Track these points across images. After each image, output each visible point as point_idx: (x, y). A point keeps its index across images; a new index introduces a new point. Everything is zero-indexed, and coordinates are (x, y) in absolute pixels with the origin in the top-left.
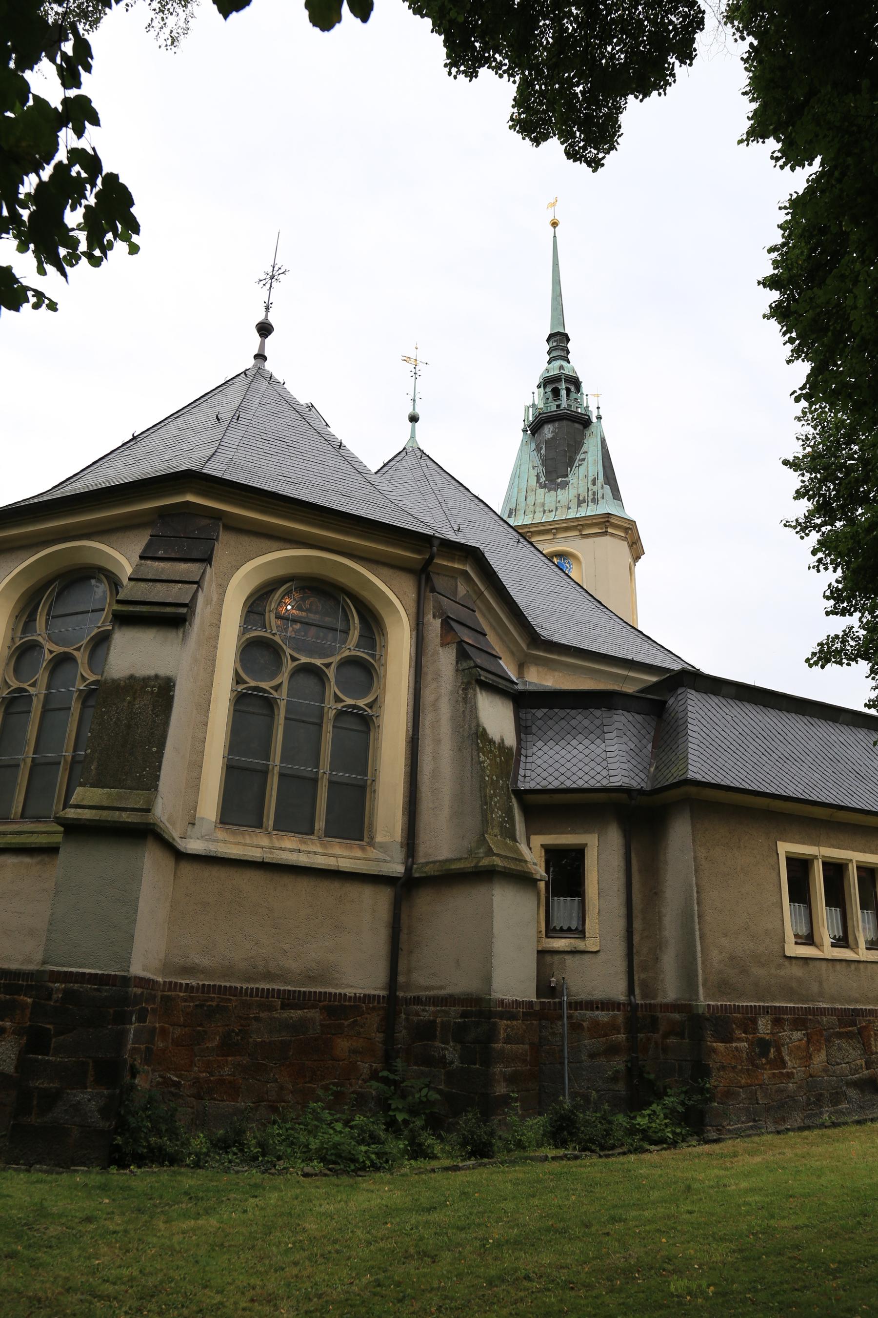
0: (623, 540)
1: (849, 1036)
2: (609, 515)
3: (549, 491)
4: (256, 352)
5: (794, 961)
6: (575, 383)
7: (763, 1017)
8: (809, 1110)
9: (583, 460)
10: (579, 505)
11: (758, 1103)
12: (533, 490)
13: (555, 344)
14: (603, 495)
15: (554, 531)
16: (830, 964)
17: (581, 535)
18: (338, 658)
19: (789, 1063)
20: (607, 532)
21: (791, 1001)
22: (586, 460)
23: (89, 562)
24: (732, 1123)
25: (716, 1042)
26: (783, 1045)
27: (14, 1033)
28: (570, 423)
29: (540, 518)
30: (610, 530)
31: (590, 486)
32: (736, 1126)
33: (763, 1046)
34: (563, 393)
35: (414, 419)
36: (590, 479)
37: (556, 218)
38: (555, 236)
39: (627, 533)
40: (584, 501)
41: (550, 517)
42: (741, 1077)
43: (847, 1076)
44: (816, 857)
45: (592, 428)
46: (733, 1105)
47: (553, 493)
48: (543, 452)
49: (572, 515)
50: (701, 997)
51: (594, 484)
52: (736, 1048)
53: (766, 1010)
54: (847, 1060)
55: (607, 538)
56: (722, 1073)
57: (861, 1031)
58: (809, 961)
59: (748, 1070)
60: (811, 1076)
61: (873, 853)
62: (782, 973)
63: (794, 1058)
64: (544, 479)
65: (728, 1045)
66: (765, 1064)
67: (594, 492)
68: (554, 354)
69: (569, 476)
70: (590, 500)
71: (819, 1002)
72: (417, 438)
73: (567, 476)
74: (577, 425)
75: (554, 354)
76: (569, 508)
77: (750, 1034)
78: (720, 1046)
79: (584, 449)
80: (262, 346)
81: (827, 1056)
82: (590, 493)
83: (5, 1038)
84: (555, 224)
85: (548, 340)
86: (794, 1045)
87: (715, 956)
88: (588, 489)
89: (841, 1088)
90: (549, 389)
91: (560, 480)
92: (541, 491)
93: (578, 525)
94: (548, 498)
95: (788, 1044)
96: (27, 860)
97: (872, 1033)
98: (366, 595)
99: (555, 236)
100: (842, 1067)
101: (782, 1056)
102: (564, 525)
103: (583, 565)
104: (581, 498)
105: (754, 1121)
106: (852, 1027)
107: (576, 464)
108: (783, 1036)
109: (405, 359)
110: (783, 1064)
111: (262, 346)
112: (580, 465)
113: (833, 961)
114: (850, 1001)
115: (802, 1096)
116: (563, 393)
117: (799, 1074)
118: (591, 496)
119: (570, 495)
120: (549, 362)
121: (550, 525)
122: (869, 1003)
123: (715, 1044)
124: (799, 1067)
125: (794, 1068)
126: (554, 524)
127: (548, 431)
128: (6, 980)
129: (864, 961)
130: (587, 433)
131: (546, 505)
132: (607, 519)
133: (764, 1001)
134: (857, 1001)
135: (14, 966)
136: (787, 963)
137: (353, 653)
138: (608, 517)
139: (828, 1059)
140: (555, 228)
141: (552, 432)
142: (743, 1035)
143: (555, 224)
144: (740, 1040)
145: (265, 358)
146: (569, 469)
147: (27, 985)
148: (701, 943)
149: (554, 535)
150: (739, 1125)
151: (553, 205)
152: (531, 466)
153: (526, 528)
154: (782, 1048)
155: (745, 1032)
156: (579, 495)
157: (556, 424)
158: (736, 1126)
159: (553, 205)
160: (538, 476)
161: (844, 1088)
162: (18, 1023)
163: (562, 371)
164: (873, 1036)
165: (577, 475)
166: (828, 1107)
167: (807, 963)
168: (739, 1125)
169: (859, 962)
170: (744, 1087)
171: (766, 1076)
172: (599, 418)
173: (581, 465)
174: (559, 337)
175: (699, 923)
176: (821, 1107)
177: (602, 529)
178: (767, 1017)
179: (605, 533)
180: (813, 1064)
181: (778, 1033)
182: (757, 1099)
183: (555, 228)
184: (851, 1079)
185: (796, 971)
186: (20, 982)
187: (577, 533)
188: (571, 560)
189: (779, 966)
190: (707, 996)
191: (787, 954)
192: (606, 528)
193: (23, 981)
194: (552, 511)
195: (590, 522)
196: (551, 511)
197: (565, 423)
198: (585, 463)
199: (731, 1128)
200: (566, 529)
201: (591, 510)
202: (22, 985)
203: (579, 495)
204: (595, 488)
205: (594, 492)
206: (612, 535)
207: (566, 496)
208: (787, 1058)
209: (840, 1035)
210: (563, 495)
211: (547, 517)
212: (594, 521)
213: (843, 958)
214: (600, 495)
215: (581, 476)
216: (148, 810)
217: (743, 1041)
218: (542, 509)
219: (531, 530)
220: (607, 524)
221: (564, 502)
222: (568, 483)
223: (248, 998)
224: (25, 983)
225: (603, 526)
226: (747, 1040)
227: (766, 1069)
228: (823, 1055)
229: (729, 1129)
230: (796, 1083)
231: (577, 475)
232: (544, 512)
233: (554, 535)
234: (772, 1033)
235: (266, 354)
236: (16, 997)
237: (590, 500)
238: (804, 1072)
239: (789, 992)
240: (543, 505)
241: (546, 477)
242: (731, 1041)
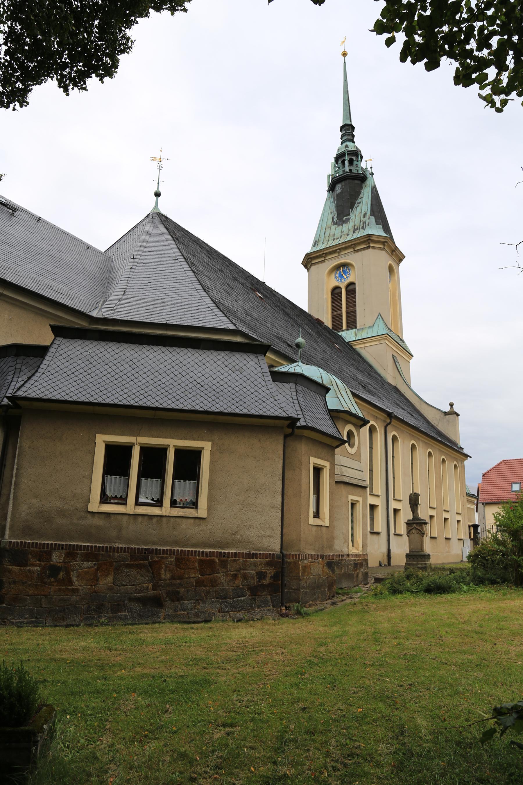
0: (382, 250)
1: (140, 567)
2: (369, 235)
3: (338, 226)
5: (96, 515)
6: (356, 154)
7: (57, 551)
8: (89, 614)
9: (360, 203)
10: (354, 232)
11: (41, 607)
12: (329, 227)
13: (344, 132)
14: (369, 223)
15: (338, 251)
16: (132, 518)
17: (355, 250)
19: (76, 583)
20: (369, 246)
21: (88, 542)
22: (361, 203)
24: (16, 618)
25: (12, 566)
26: (73, 571)
28: (351, 181)
29: (331, 243)
30: (372, 245)
31: (362, 219)
32: (19, 620)
33: (54, 570)
34: (347, 162)
35: (158, 195)
36: (363, 214)
38: (345, 62)
39: (384, 245)
40: (357, 229)
41: (336, 242)
42: (29, 589)
43: (131, 594)
44: (133, 444)
45: (368, 182)
46: (19, 607)
47: (340, 227)
48: (336, 202)
49: (349, 238)
50: (7, 536)
51: (364, 216)
52: (29, 570)
53: (61, 547)
54: (133, 583)
55: (370, 250)
56: (12, 586)
57: (151, 565)
58: (111, 515)
59: (36, 585)
60: (95, 592)
61: (194, 440)
62: (84, 522)
63: (82, 579)
64: (336, 219)
65: (22, 568)
66: (53, 582)
67: (364, 222)
68: (344, 138)
69: (351, 214)
70: (361, 228)
71: (116, 543)
72: (159, 207)
73: (349, 215)
74: (356, 182)
75: (344, 138)
76: (348, 235)
77: (43, 562)
78: (15, 568)
79: (361, 196)
81: (114, 579)
82: (362, 223)
84: (344, 55)
85: (341, 131)
86: (83, 572)
87: (24, 510)
88: (361, 221)
89: (124, 601)
90: (340, 162)
91: (345, 218)
92: (334, 227)
93: (352, 245)
94: (337, 230)
95: (77, 570)
97: (163, 566)
99: (345, 62)
100: (127, 588)
101: (71, 578)
102: (344, 246)
103: (356, 270)
104: (356, 227)
105: (36, 618)
106: (144, 560)
107: (355, 206)
108: (74, 564)
109: (153, 159)
110: (71, 582)
112: (357, 206)
113: (135, 515)
114: (146, 543)
115: (84, 605)
116: (347, 162)
117: (84, 590)
118: (362, 225)
119: (350, 226)
120: (341, 144)
121: (336, 247)
122: (167, 545)
123: (10, 567)
124: (85, 585)
125: (80, 586)
126: (338, 247)
127: (338, 189)
129: (166, 516)
130: (364, 185)
131: (335, 235)
132: (368, 238)
133: (62, 541)
134: (154, 543)
136: (89, 516)
138: (369, 237)
139: (114, 582)
140: (345, 57)
141: (341, 189)
142: (38, 562)
143: (344, 55)
144: (33, 565)
146: (351, 210)
148: (13, 502)
149: (339, 253)
150: (22, 620)
151: (344, 42)
152: (330, 212)
153: (321, 252)
154: (72, 573)
155: (39, 560)
156: (355, 226)
157: (343, 183)
158: (19, 620)
159: (344, 42)
160: (333, 218)
161: (126, 602)
163: (347, 149)
164: (164, 567)
165: (355, 213)
166: (108, 613)
167: (109, 516)
168: (22, 620)
169: (162, 516)
170: (31, 596)
171: (52, 590)
172: (372, 174)
173: (358, 206)
174: (346, 127)
175: (14, 489)
176: (102, 613)
177: (367, 245)
178: (61, 552)
179: (369, 247)
180: (99, 584)
181: (70, 562)
182: (41, 604)
183: (345, 57)
184: (135, 596)
185: (97, 522)
187: (352, 250)
188: (350, 267)
189: (81, 518)
190: (11, 536)
191: (89, 510)
192: (369, 244)
194: (338, 238)
195: (359, 241)
196: (337, 239)
197: (348, 181)
198: (360, 205)
199: (14, 621)
200: (346, 248)
201: (362, 233)
203: (355, 226)
204: (364, 220)
205: (364, 222)
206: (374, 248)
207: (348, 227)
208: (75, 579)
209: (128, 566)
210: (346, 227)
211: (335, 242)
212: (361, 240)
213: (144, 514)
214: (367, 223)
215: (358, 213)
217: (36, 566)
218: (333, 238)
219: (325, 252)
220: (369, 241)
221: (346, 232)
222: (349, 219)
225: (367, 243)
226: (40, 566)
227: (53, 585)
228: (110, 579)
229: (12, 622)
230: (80, 596)
231: (355, 213)
232: (334, 239)
233: (339, 253)
234: (64, 562)
237: (361, 228)
238: (89, 589)
239: (86, 534)
240: (334, 235)
241: (337, 217)
242: (26, 565)
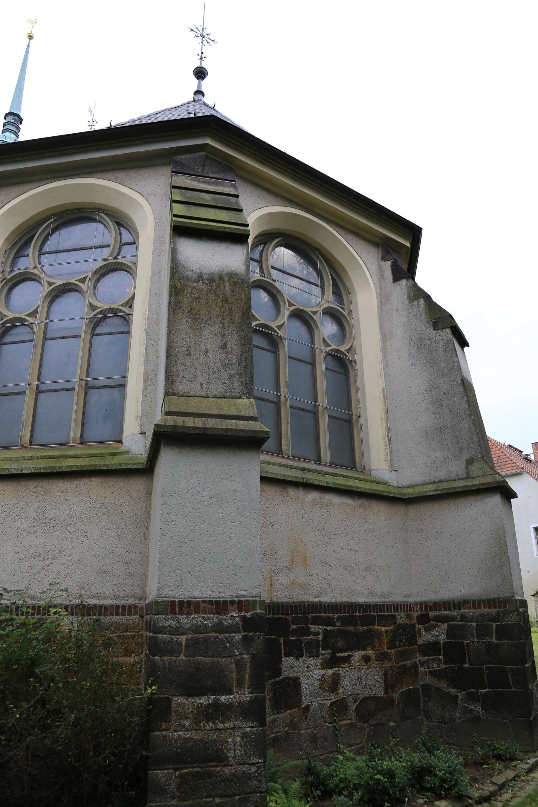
4: (196, 90)
18: (322, 308)
23: (319, 241)
27: (376, 660)
37: (32, 33)
80: (199, 85)
83: (370, 666)
84: (30, 37)
85: (6, 116)
96: (349, 501)
98: (340, 257)
111: (199, 85)
128: (360, 612)
135: (361, 600)
137: (331, 305)
143: (30, 37)
145: (203, 94)
147: (378, 615)
162: (378, 650)
183: (30, 39)
186: (372, 614)
193: (374, 612)
202: (374, 616)
216: (120, 440)
223: (412, 613)
224: (376, 614)
235: (203, 90)
236: (371, 627)
